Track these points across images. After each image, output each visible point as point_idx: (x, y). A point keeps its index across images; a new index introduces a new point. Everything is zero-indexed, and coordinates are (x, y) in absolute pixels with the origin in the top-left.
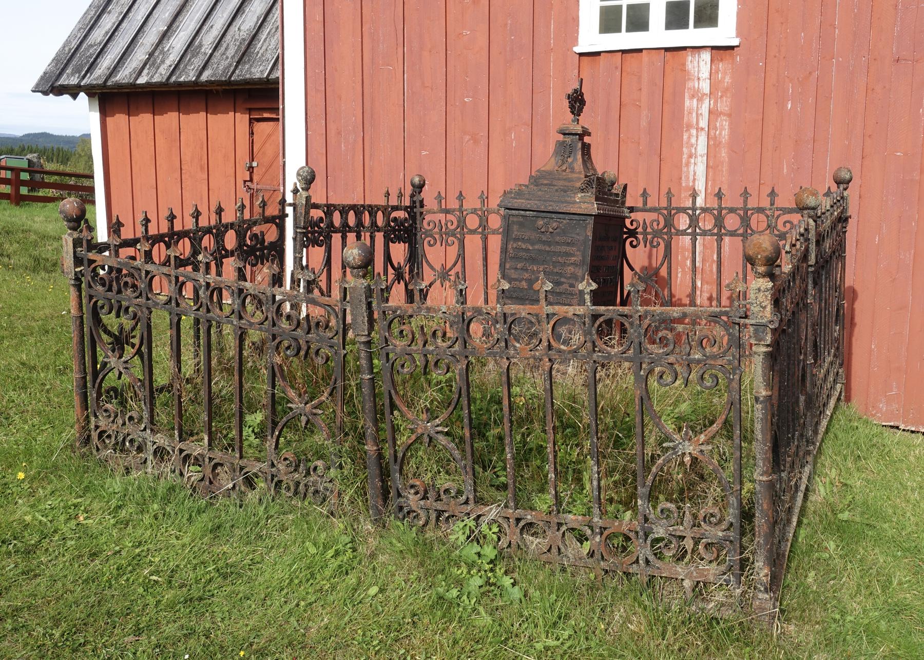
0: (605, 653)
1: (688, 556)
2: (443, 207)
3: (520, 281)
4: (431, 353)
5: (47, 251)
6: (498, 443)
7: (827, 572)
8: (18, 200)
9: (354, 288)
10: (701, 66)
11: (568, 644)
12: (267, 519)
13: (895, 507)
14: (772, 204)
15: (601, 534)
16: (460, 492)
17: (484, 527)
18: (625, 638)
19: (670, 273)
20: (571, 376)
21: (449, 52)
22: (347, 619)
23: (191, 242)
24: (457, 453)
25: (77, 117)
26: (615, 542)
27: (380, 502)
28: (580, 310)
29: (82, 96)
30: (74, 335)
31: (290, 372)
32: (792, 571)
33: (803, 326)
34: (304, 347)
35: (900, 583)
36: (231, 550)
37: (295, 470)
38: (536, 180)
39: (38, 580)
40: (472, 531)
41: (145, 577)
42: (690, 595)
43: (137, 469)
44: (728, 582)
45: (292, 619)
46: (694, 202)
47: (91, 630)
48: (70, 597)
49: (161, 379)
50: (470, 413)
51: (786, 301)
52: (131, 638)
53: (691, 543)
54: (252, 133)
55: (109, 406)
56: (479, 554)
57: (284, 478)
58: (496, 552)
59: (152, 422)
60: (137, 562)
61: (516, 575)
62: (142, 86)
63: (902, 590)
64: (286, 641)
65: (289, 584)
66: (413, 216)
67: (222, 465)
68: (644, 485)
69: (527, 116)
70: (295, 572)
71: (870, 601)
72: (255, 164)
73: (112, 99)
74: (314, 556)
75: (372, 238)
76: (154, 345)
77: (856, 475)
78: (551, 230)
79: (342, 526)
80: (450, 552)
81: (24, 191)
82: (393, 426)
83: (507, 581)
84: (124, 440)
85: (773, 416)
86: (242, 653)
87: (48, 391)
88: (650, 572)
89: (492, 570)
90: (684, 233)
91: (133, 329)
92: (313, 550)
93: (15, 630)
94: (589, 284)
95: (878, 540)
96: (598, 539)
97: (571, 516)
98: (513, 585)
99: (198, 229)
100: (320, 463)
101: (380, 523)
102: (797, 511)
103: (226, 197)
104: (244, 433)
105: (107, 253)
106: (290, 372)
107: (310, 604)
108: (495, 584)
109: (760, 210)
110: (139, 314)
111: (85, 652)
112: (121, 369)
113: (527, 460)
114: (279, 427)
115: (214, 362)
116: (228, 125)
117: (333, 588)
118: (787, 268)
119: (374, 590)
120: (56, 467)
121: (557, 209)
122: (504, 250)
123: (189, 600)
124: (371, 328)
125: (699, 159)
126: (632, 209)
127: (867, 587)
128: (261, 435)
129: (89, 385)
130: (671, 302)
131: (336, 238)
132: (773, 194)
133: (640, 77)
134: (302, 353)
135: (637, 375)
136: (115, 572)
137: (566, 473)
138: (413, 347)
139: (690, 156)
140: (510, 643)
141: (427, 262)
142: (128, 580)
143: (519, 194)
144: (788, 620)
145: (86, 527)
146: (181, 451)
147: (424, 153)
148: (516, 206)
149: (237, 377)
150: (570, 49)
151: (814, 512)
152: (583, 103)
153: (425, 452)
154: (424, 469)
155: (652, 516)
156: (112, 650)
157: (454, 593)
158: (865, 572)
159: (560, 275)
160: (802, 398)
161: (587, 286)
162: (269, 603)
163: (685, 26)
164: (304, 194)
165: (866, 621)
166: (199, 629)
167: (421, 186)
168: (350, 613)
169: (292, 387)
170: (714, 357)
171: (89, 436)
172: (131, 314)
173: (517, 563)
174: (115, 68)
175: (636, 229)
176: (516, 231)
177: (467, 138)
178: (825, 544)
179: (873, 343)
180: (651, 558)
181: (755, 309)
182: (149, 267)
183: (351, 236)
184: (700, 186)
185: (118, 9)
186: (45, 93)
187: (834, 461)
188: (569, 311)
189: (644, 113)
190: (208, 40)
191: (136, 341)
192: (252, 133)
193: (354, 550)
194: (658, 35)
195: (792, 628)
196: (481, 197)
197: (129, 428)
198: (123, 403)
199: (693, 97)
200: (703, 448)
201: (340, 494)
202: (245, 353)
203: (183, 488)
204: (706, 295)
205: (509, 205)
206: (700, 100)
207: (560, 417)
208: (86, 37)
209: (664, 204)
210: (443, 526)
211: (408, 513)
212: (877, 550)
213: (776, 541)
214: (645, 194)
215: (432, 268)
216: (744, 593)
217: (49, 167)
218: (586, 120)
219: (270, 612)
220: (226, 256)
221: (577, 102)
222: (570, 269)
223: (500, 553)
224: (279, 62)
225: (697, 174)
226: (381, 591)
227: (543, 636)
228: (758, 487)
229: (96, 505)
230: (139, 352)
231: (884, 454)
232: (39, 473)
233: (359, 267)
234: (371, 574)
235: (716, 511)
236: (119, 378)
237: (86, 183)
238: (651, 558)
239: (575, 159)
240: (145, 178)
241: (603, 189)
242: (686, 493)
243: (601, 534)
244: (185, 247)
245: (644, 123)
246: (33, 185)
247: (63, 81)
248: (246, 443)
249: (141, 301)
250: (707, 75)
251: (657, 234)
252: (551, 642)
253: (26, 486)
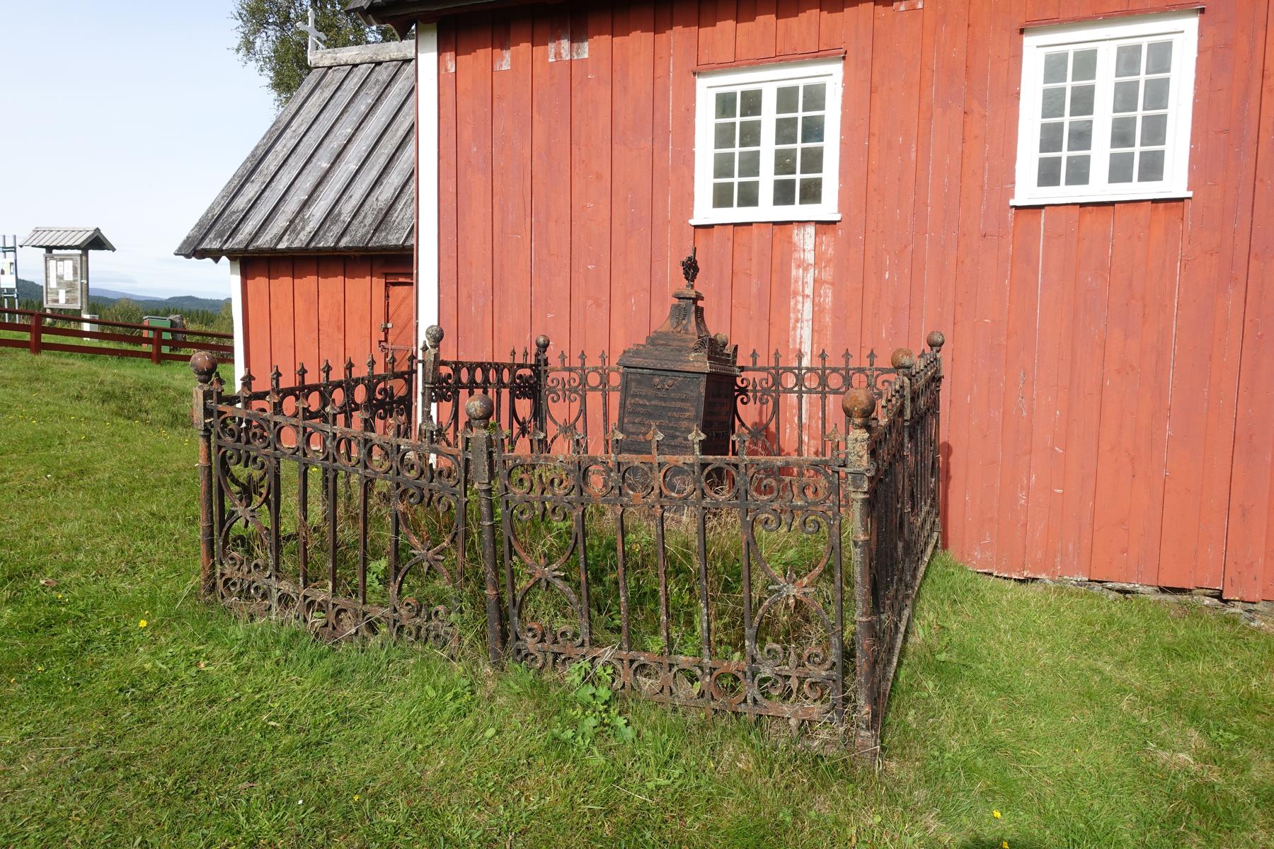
0: (714, 791)
1: (794, 696)
2: (567, 365)
4: (549, 500)
5: (183, 408)
6: (613, 587)
7: (927, 711)
8: (159, 358)
9: (476, 439)
10: (806, 239)
11: (679, 783)
12: (389, 663)
13: (989, 648)
14: (871, 365)
15: (711, 674)
16: (576, 635)
17: (599, 669)
18: (734, 776)
19: (778, 428)
20: (684, 524)
22: (463, 761)
23: (319, 395)
24: (573, 597)
25: (219, 281)
26: (725, 682)
27: (499, 645)
28: (690, 459)
29: (224, 259)
30: (201, 486)
31: (414, 520)
32: (893, 708)
33: (900, 477)
34: (427, 495)
35: (995, 721)
36: (352, 695)
37: (417, 615)
38: (652, 341)
39: (154, 728)
40: (587, 673)
41: (264, 723)
42: (796, 733)
43: (262, 616)
44: (831, 720)
45: (409, 763)
46: (800, 363)
47: (205, 777)
48: (184, 744)
49: (288, 527)
50: (586, 558)
51: (883, 452)
52: (246, 785)
53: (796, 682)
54: (387, 297)
55: (235, 554)
56: (594, 695)
57: (406, 623)
58: (610, 693)
59: (277, 570)
60: (256, 708)
61: (629, 716)
62: (282, 251)
63: (997, 727)
64: (401, 784)
65: (408, 727)
66: (537, 374)
67: (345, 611)
68: (751, 627)
69: (646, 284)
70: (414, 714)
71: (967, 737)
72: (389, 325)
73: (252, 262)
74: (432, 700)
75: (499, 394)
76: (283, 496)
77: (953, 618)
79: (461, 669)
80: (566, 693)
81: (165, 350)
82: (512, 571)
83: (621, 722)
84: (249, 587)
85: (871, 560)
86: (356, 798)
87: (176, 541)
88: (757, 710)
89: (606, 711)
90: (791, 391)
91: (262, 479)
92: (432, 693)
93: (127, 778)
94: (698, 435)
95: (974, 680)
96: (708, 679)
97: (682, 657)
98: (627, 725)
99: (328, 383)
100: (441, 608)
101: (499, 666)
102: (897, 651)
103: (364, 357)
104: (368, 580)
105: (239, 405)
106: (414, 520)
107: (428, 747)
108: (608, 725)
109: (861, 370)
110: (267, 463)
111: (198, 800)
112: (249, 519)
113: (641, 604)
114: (402, 573)
115: (340, 510)
116: (364, 290)
117: (451, 730)
118: (883, 421)
119: (490, 732)
120: (179, 616)
122: (623, 406)
123: (306, 746)
124: (492, 475)
125: (805, 324)
126: (742, 369)
127: (964, 725)
128: (384, 581)
129: (216, 533)
130: (780, 452)
131: (464, 393)
132: (872, 355)
133: (750, 248)
134: (426, 500)
135: (743, 520)
136: (233, 718)
137: (678, 616)
138: (532, 495)
139: (797, 321)
140: (623, 783)
141: (551, 417)
142: (246, 726)
143: (637, 353)
144: (890, 757)
145: (207, 674)
146: (306, 597)
148: (634, 364)
149: (361, 525)
151: (914, 653)
152: (696, 270)
153: (543, 595)
154: (541, 613)
155: (759, 656)
156: (225, 797)
157: (569, 733)
158: (962, 711)
159: (675, 429)
160: (900, 545)
161: (696, 436)
162: (386, 746)
163: (792, 202)
164: (433, 351)
165: (964, 758)
166: (315, 774)
167: (546, 346)
168: (467, 755)
169: (416, 534)
170: (815, 504)
171: (214, 584)
173: (631, 704)
174: (257, 233)
176: (634, 388)
177: (590, 302)
178: (924, 683)
179: (968, 495)
180: (759, 697)
181: (852, 458)
182: (278, 419)
183: (478, 392)
184: (806, 348)
185: (261, 179)
186: (188, 256)
187: (931, 605)
188: (680, 459)
190: (347, 209)
191: (264, 491)
192: (387, 297)
193: (473, 693)
194: (766, 210)
195: (893, 765)
196: (601, 356)
197: (255, 575)
198: (249, 551)
199: (798, 267)
200: (807, 590)
201: (460, 638)
202: (371, 502)
203: (305, 634)
204: (813, 450)
205: (628, 364)
206: (806, 270)
207: (673, 563)
208: (229, 204)
209: (772, 364)
210: (560, 669)
211: (526, 656)
212: (973, 690)
213: (876, 680)
214: (754, 355)
215: (555, 422)
216: (847, 731)
217: (192, 327)
218: (700, 284)
219: (387, 756)
220: (357, 409)
221: (691, 268)
222: (685, 424)
223: (614, 694)
224: (413, 231)
225: (804, 337)
226: (498, 733)
227: (655, 775)
228: (858, 628)
229: (218, 652)
230: (266, 500)
231: (979, 598)
232: (162, 621)
233: (481, 418)
234: (488, 715)
235: (819, 650)
236: (246, 526)
237: (227, 343)
238: (759, 697)
239: (689, 321)
240: (283, 337)
241: (715, 349)
242: (793, 634)
243: (711, 674)
244: (314, 401)
245: (754, 290)
246: (174, 344)
247: (204, 246)
248: (369, 589)
249: (270, 450)
250: (812, 246)
251: (766, 391)
252: (662, 781)
253: (148, 634)
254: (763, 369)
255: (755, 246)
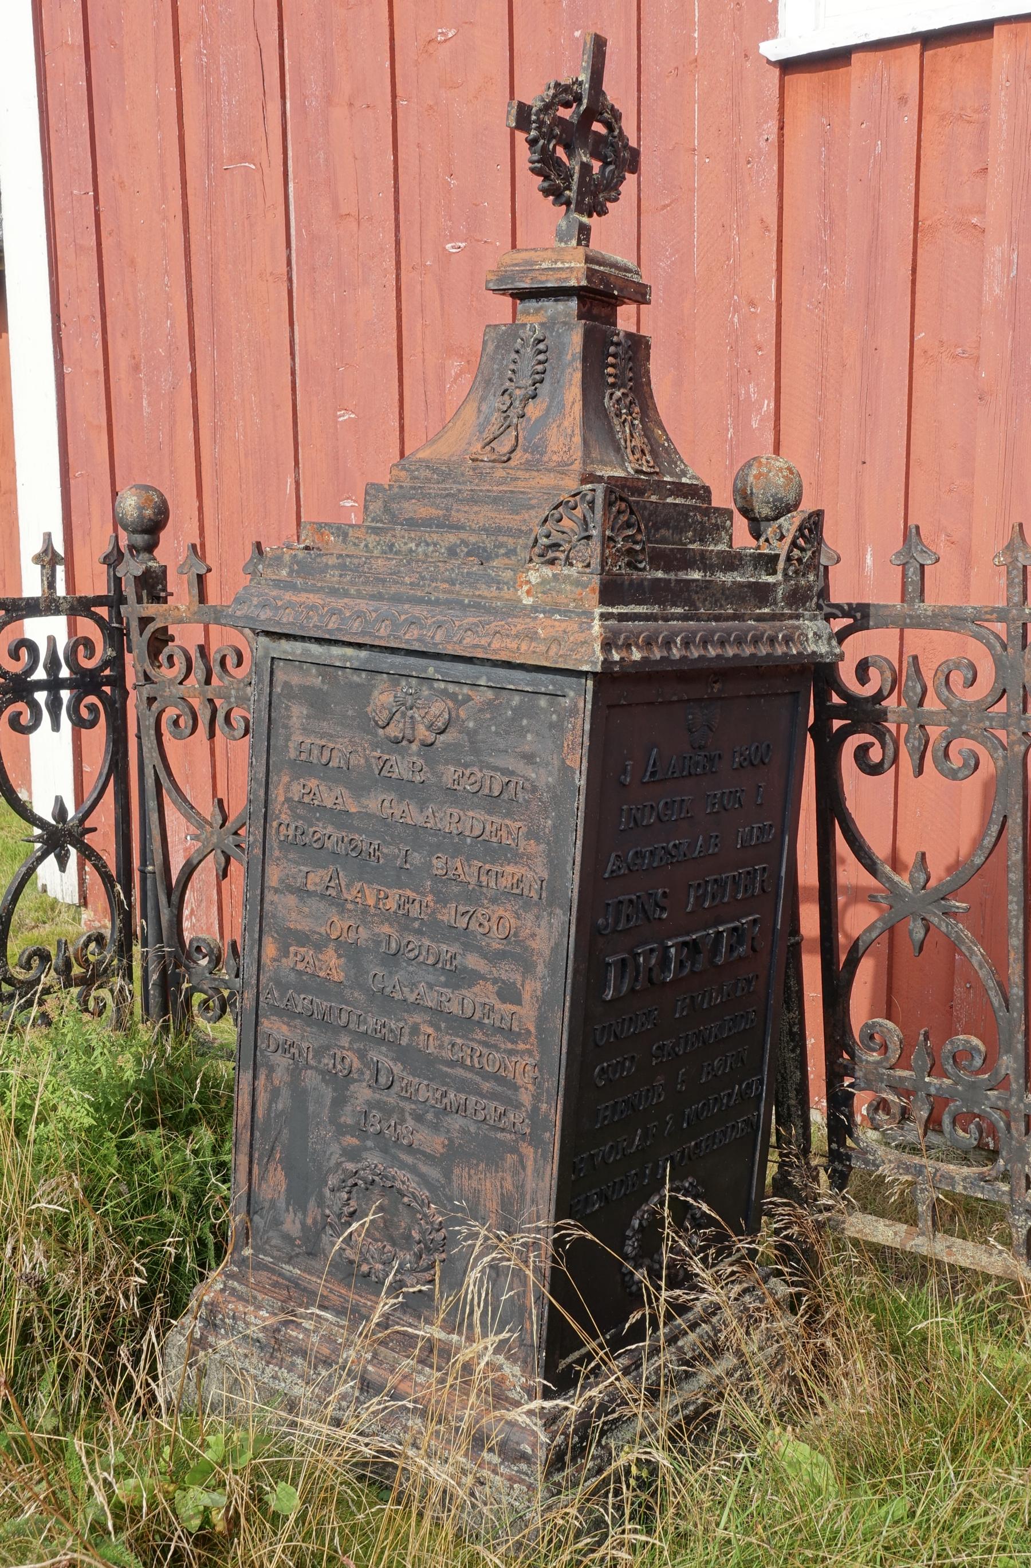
3: (319, 947)
21: (401, 103)
78: (422, 733)
121: (439, 640)
133: (984, 126)
147: (344, 417)
150: (749, 53)
172: (239, 725)
175: (879, 697)
189: (997, 251)
239: (556, 407)
241: (651, 532)
245: (995, 289)
254: (953, 620)
255: (1001, 118)
